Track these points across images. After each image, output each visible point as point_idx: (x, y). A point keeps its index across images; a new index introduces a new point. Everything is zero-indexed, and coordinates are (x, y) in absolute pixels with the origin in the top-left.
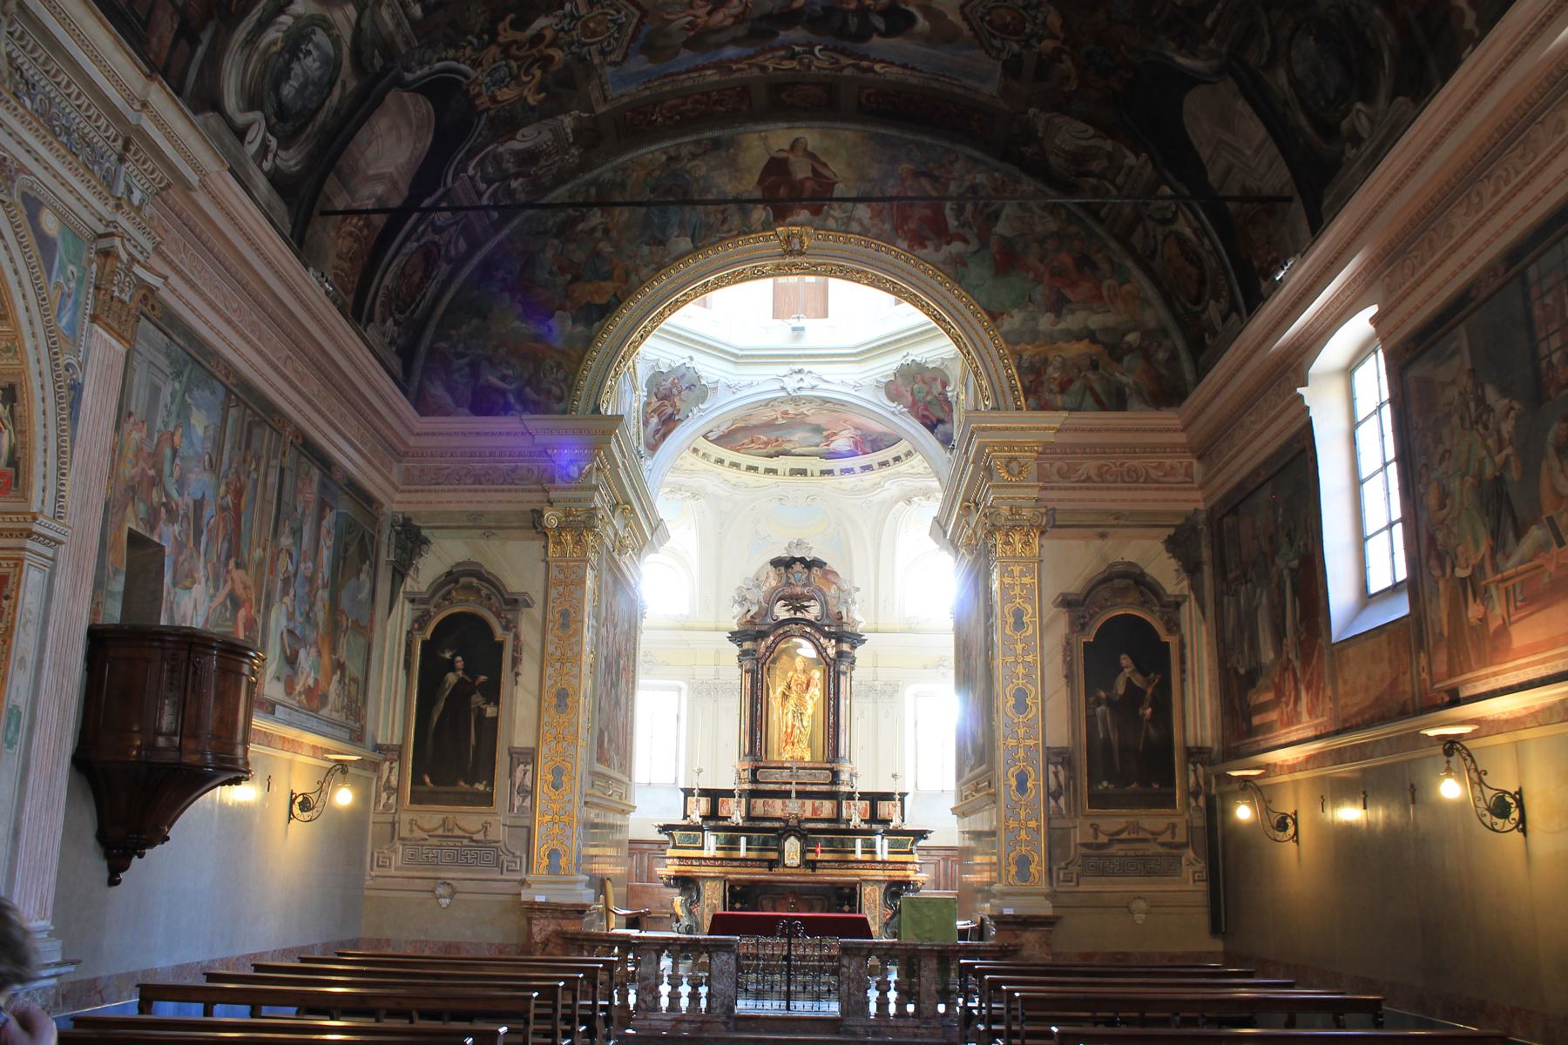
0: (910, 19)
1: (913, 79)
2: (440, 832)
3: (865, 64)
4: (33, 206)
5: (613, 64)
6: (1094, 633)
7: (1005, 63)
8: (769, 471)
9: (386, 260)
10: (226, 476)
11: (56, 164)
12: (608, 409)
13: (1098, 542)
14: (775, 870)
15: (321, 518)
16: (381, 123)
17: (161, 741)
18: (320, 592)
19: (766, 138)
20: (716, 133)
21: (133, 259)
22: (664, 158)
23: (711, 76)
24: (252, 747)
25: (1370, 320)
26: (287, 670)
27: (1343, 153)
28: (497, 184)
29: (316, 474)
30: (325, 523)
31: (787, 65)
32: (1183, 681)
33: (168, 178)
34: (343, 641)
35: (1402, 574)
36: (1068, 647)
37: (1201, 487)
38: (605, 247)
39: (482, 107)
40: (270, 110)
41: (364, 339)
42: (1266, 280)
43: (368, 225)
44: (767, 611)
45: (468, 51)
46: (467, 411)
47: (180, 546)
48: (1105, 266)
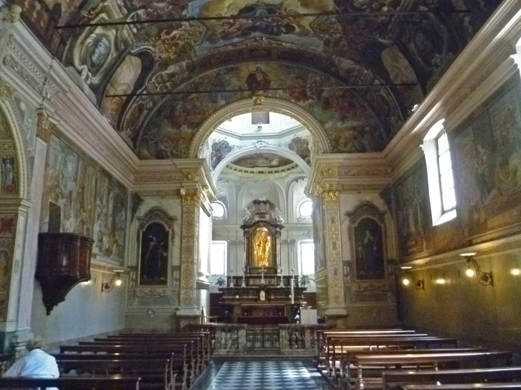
0: (294, 28)
1: (295, 47)
3: (279, 43)
4: (18, 101)
5: (198, 45)
6: (357, 224)
7: (324, 42)
8: (251, 172)
11: (25, 88)
12: (201, 157)
13: (358, 195)
15: (109, 194)
17: (63, 269)
20: (232, 66)
21: (48, 116)
22: (215, 74)
23: (230, 48)
24: (91, 269)
25: (442, 124)
26: (99, 244)
27: (432, 70)
29: (107, 180)
31: (254, 43)
33: (58, 89)
36: (349, 229)
38: (198, 104)
39: (156, 60)
40: (89, 63)
41: (120, 136)
43: (121, 99)
45: (152, 43)
47: (65, 206)
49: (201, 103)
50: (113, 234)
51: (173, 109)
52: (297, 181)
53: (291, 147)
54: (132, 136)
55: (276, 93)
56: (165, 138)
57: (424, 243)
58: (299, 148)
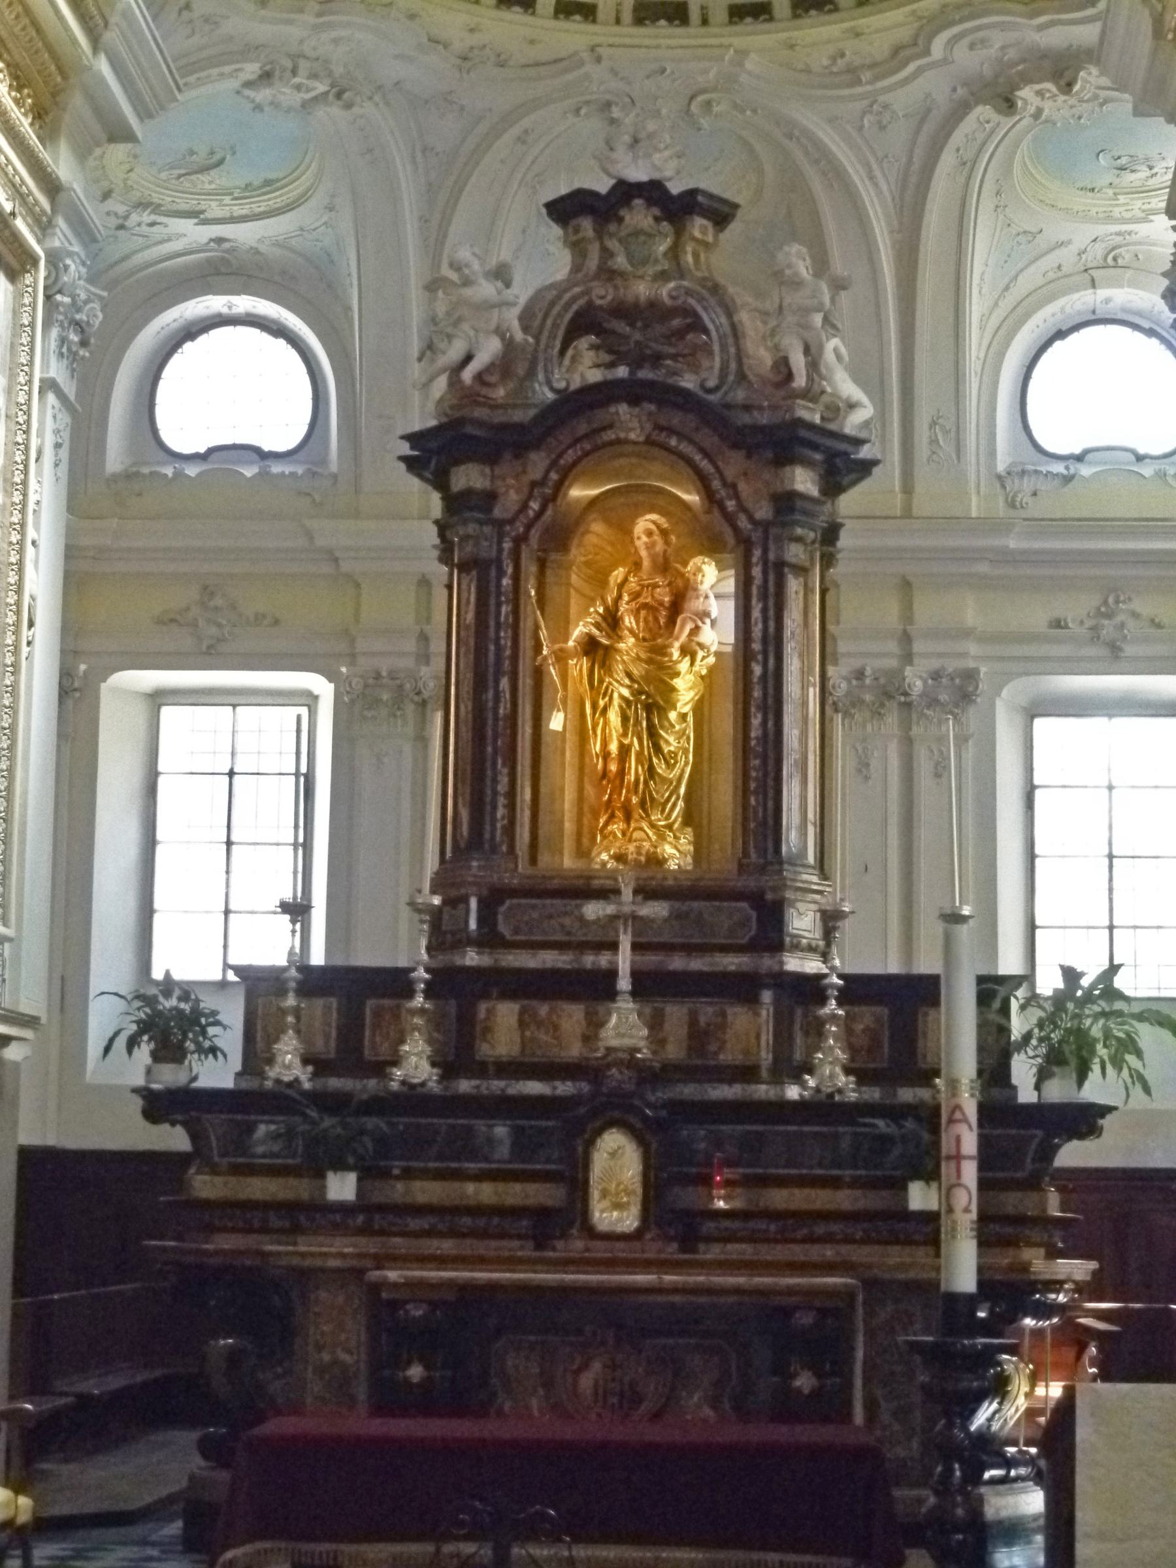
14: (561, 1249)
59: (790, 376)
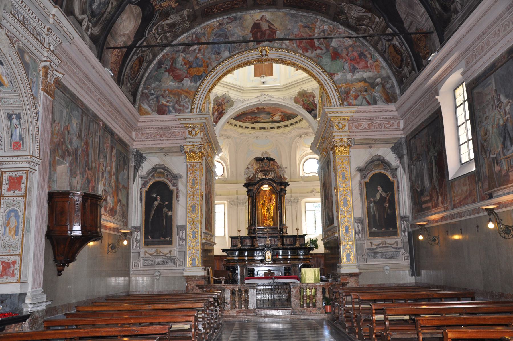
2: (155, 254)
8: (252, 128)
9: (127, 63)
10: (83, 140)
13: (369, 149)
15: (112, 152)
16: (124, 16)
18: (113, 177)
19: (252, 16)
22: (218, 24)
28: (162, 35)
29: (109, 137)
30: (113, 153)
32: (399, 194)
34: (120, 192)
35: (472, 156)
37: (403, 129)
38: (200, 56)
39: (157, 9)
40: (89, 13)
42: (424, 60)
44: (255, 176)
46: (156, 113)
48: (369, 56)
49: (203, 55)
50: (116, 193)
51: (174, 61)
52: (300, 137)
53: (296, 101)
54: (132, 90)
55: (282, 43)
56: (167, 92)
57: (440, 198)
58: (305, 102)
59: (281, 177)
